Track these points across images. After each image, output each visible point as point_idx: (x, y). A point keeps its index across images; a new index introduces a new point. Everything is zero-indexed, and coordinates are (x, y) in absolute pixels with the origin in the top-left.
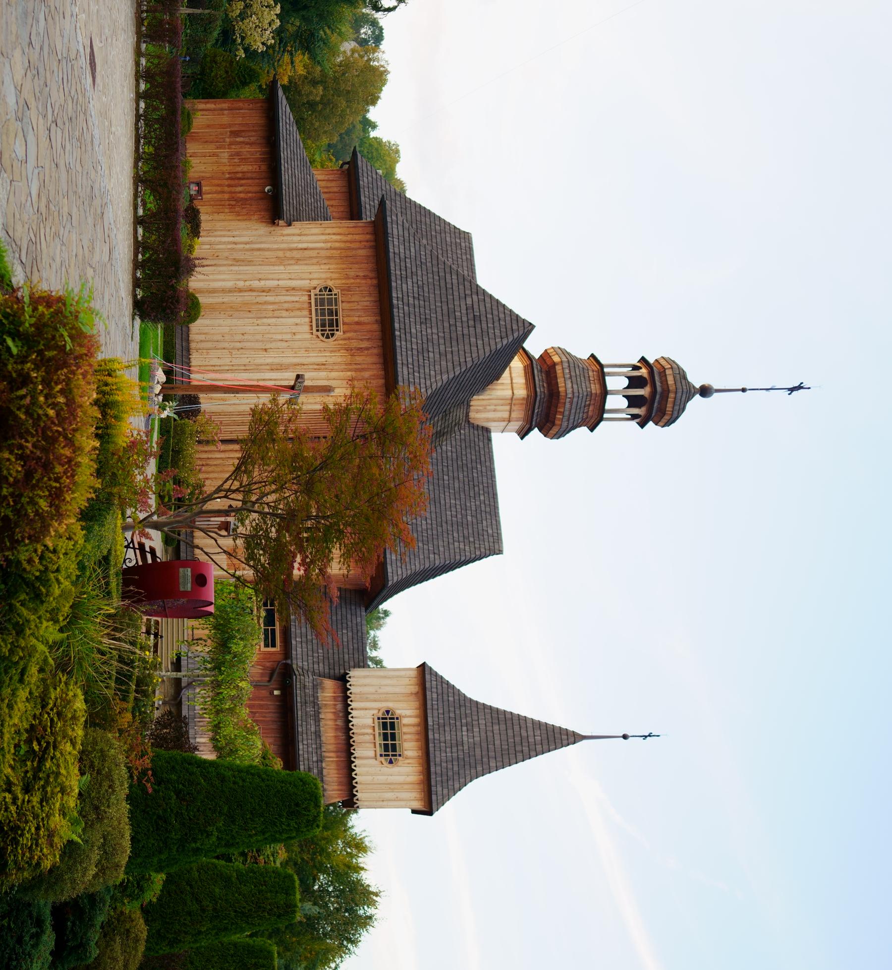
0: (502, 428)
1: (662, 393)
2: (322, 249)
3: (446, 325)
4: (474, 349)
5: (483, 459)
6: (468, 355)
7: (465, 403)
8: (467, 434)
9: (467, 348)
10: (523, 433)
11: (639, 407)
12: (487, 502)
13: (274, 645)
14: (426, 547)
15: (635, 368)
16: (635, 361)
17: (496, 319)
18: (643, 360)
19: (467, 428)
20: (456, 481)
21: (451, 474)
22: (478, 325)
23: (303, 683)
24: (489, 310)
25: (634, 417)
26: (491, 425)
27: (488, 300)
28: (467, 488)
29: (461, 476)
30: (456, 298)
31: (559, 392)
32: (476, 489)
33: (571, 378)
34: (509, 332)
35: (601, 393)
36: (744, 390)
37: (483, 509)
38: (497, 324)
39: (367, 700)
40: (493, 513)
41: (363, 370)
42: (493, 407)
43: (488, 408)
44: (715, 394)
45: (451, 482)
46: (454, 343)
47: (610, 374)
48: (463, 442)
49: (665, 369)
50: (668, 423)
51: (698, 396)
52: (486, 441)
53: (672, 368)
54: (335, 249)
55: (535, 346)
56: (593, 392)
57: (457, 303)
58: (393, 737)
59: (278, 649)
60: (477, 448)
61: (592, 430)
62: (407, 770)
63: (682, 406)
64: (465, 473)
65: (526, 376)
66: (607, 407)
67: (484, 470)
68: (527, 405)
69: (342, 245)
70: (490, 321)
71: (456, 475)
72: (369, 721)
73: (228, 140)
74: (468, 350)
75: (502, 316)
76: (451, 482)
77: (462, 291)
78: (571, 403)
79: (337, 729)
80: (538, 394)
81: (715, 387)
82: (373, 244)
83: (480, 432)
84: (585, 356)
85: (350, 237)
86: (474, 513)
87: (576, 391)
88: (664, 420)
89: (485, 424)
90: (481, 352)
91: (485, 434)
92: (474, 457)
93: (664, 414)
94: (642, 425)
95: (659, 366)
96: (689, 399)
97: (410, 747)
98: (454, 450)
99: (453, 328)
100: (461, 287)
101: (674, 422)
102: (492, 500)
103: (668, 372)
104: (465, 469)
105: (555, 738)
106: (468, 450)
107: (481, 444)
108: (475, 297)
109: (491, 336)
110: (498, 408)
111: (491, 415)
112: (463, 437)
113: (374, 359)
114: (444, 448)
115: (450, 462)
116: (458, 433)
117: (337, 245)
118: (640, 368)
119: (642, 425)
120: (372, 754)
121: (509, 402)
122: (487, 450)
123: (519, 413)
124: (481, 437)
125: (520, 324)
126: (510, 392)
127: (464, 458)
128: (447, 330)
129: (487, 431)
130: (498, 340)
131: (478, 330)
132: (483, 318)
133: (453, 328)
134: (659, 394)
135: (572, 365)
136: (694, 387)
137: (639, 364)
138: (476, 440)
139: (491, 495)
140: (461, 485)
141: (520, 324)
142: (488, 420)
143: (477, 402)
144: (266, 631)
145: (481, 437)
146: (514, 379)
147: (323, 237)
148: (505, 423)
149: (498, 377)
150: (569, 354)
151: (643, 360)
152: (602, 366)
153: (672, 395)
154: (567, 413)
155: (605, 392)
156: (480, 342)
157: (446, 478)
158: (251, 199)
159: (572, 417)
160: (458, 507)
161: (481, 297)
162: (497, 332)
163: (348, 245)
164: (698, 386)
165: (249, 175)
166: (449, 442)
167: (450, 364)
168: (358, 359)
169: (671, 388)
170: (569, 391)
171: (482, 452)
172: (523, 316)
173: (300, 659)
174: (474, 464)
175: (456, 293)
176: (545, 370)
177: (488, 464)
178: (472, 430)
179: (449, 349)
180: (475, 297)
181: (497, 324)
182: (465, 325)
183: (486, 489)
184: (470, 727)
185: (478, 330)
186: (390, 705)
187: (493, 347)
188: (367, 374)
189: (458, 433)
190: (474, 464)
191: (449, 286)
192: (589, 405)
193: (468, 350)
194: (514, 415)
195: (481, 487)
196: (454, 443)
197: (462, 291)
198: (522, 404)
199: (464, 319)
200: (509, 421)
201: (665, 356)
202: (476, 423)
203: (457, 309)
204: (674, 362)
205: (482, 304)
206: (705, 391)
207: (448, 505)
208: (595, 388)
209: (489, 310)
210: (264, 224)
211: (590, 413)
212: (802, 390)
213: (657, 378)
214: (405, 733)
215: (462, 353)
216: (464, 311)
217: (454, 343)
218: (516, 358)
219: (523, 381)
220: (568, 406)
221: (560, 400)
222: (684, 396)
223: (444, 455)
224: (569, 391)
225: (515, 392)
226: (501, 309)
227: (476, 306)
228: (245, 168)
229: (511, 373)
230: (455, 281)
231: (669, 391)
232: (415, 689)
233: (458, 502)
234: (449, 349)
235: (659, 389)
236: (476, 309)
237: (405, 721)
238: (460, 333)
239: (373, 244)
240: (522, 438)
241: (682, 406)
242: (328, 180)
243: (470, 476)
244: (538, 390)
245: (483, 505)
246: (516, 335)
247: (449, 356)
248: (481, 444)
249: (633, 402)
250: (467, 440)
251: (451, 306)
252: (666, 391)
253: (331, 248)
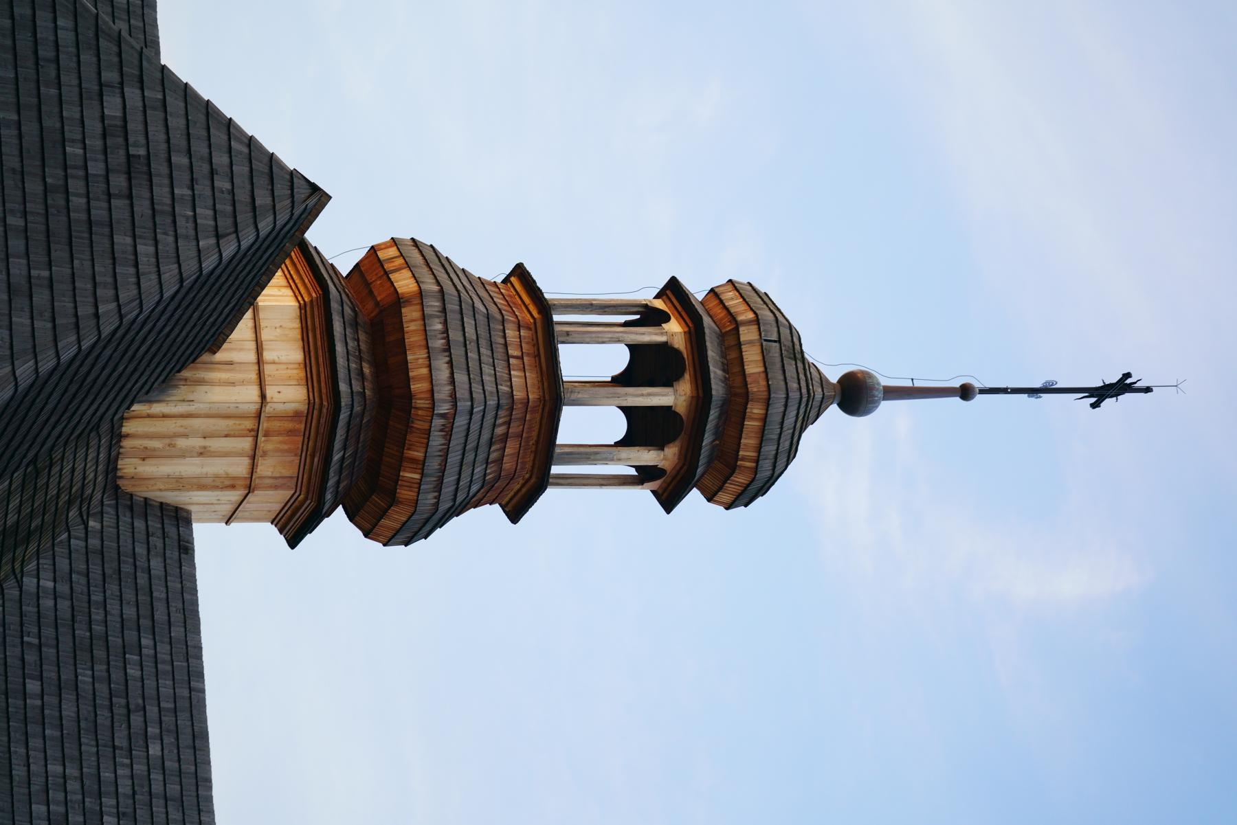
0: (228, 509)
1: (726, 405)
3: (34, 187)
4: (125, 271)
5: (160, 615)
6: (105, 293)
7: (105, 427)
8: (110, 531)
9: (103, 267)
10: (296, 527)
12: (171, 765)
14: (139, 524)
15: (649, 316)
16: (646, 292)
17: (202, 169)
18: (673, 289)
19: (110, 511)
20: (69, 697)
21: (50, 673)
22: (141, 192)
24: (178, 139)
25: (645, 475)
26: (191, 499)
27: (175, 104)
28: (103, 717)
29: (85, 678)
30: (70, 93)
31: (409, 396)
32: (136, 719)
33: (448, 349)
34: (244, 217)
35: (542, 399)
36: (965, 392)
37: (157, 788)
38: (203, 188)
40: (189, 801)
42: (197, 442)
43: (182, 443)
44: (886, 407)
45: (51, 700)
46: (59, 252)
47: (569, 338)
48: (95, 560)
49: (737, 325)
50: (745, 497)
51: (834, 410)
52: (173, 554)
53: (757, 321)
55: (338, 240)
56: (519, 394)
57: (71, 112)
60: (142, 580)
61: (515, 514)
63: (785, 445)
64: (100, 668)
65: (305, 338)
66: (565, 436)
67: (163, 654)
68: (306, 435)
70: (182, 177)
71: (67, 675)
74: (104, 278)
75: (220, 159)
76: (51, 700)
77: (89, 72)
78: (448, 432)
80: (345, 400)
81: (886, 379)
83: (154, 524)
84: (494, 270)
86: (125, 804)
87: (462, 393)
88: (732, 488)
89: (172, 497)
90: (149, 282)
91: (171, 531)
92: (130, 612)
93: (733, 468)
94: (669, 500)
95: (719, 313)
96: (806, 420)
98: (63, 588)
99: (57, 200)
100: (87, 57)
101: (763, 490)
102: (187, 755)
103: (748, 334)
104: (99, 653)
106: (112, 588)
107: (156, 564)
108: (132, 94)
109: (184, 227)
110: (216, 444)
111: (190, 468)
112: (94, 542)
114: (29, 583)
115: (48, 632)
116: (78, 531)
118: (667, 319)
119: (669, 500)
121: (249, 424)
122: (174, 585)
123: (278, 464)
124: (156, 541)
125: (281, 189)
126: (253, 393)
127: (98, 615)
128: (35, 207)
129: (180, 519)
130: (206, 242)
131: (142, 207)
132: (159, 167)
133: (57, 200)
134: (720, 402)
135: (452, 306)
136: (822, 380)
137: (659, 304)
138: (141, 550)
139: (185, 739)
140: (86, 709)
141: (281, 189)
142: (181, 483)
143: (145, 424)
145: (156, 541)
146: (267, 350)
148: (235, 496)
149: (216, 338)
150: (446, 264)
151: (673, 289)
152: (545, 307)
153: (755, 410)
154: (433, 464)
155: (555, 393)
156: (145, 249)
157: (33, 686)
159: (450, 479)
160: (73, 786)
161: (153, 94)
162: (204, 212)
164: (833, 376)
166: (46, 562)
167: (43, 325)
169: (753, 388)
170: (443, 392)
171: (159, 593)
172: (291, 159)
174: (131, 635)
175: (69, 79)
176: (371, 315)
177: (177, 632)
178: (125, 519)
179: (41, 273)
180: (132, 94)
181: (203, 188)
182: (98, 188)
183: (168, 719)
185: (142, 207)
187: (190, 267)
189: (78, 531)
190: (131, 635)
191: (46, 52)
192: (505, 438)
193: (104, 278)
194: (266, 468)
195: (152, 711)
196: (63, 564)
197: (89, 72)
198: (290, 432)
199: (96, 168)
200: (250, 489)
201: (741, 278)
202: (142, 492)
203: (72, 132)
204: (765, 299)
205: (155, 117)
206: (856, 394)
207: (37, 784)
208: (523, 383)
209: (178, 139)
211: (508, 464)
212: (1127, 398)
213: (712, 354)
214: (743, 459)
215: (83, 285)
216: (95, 143)
217: (59, 252)
218: (278, 278)
219: (298, 356)
220: (437, 441)
221: (419, 410)
222: (792, 414)
223: (29, 609)
224: (443, 392)
225: (270, 392)
226: (219, 137)
227: (135, 125)
229: (256, 329)
230: (66, 37)
231: (746, 397)
233: (72, 771)
234: (41, 273)
235: (717, 390)
236: (136, 136)
238: (79, 216)
240: (293, 542)
241: (785, 445)
243: (116, 675)
244: (343, 387)
245: (156, 776)
246: (265, 225)
247: (41, 297)
248: (156, 564)
249: (644, 427)
250: (111, 554)
251: (50, 122)
252: (738, 396)
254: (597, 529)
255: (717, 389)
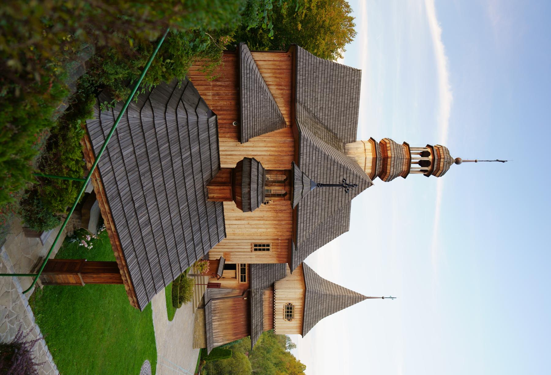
2: (265, 155)
11: (427, 166)
13: (245, 281)
23: (255, 297)
36: (476, 161)
39: (282, 300)
41: (282, 220)
44: (463, 163)
51: (454, 164)
54: (272, 155)
58: (291, 312)
59: (246, 282)
62: (295, 322)
69: (276, 154)
72: (282, 307)
73: (211, 83)
79: (269, 303)
81: (463, 159)
82: (293, 153)
85: (280, 149)
97: (297, 316)
101: (443, 174)
105: (356, 298)
113: (288, 215)
117: (273, 153)
120: (282, 317)
135: (396, 159)
144: (242, 276)
147: (266, 149)
158: (225, 123)
163: (280, 153)
164: (454, 158)
165: (225, 108)
168: (280, 215)
173: (255, 285)
184: (322, 304)
186: (291, 302)
188: (283, 223)
206: (457, 162)
210: (233, 140)
213: (436, 163)
228: (222, 103)
232: (301, 296)
237: (296, 307)
239: (293, 153)
242: (280, 61)
253: (270, 155)
254: (416, 178)
255: (436, 158)
